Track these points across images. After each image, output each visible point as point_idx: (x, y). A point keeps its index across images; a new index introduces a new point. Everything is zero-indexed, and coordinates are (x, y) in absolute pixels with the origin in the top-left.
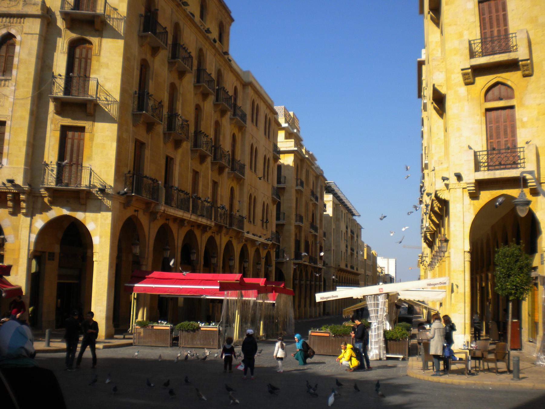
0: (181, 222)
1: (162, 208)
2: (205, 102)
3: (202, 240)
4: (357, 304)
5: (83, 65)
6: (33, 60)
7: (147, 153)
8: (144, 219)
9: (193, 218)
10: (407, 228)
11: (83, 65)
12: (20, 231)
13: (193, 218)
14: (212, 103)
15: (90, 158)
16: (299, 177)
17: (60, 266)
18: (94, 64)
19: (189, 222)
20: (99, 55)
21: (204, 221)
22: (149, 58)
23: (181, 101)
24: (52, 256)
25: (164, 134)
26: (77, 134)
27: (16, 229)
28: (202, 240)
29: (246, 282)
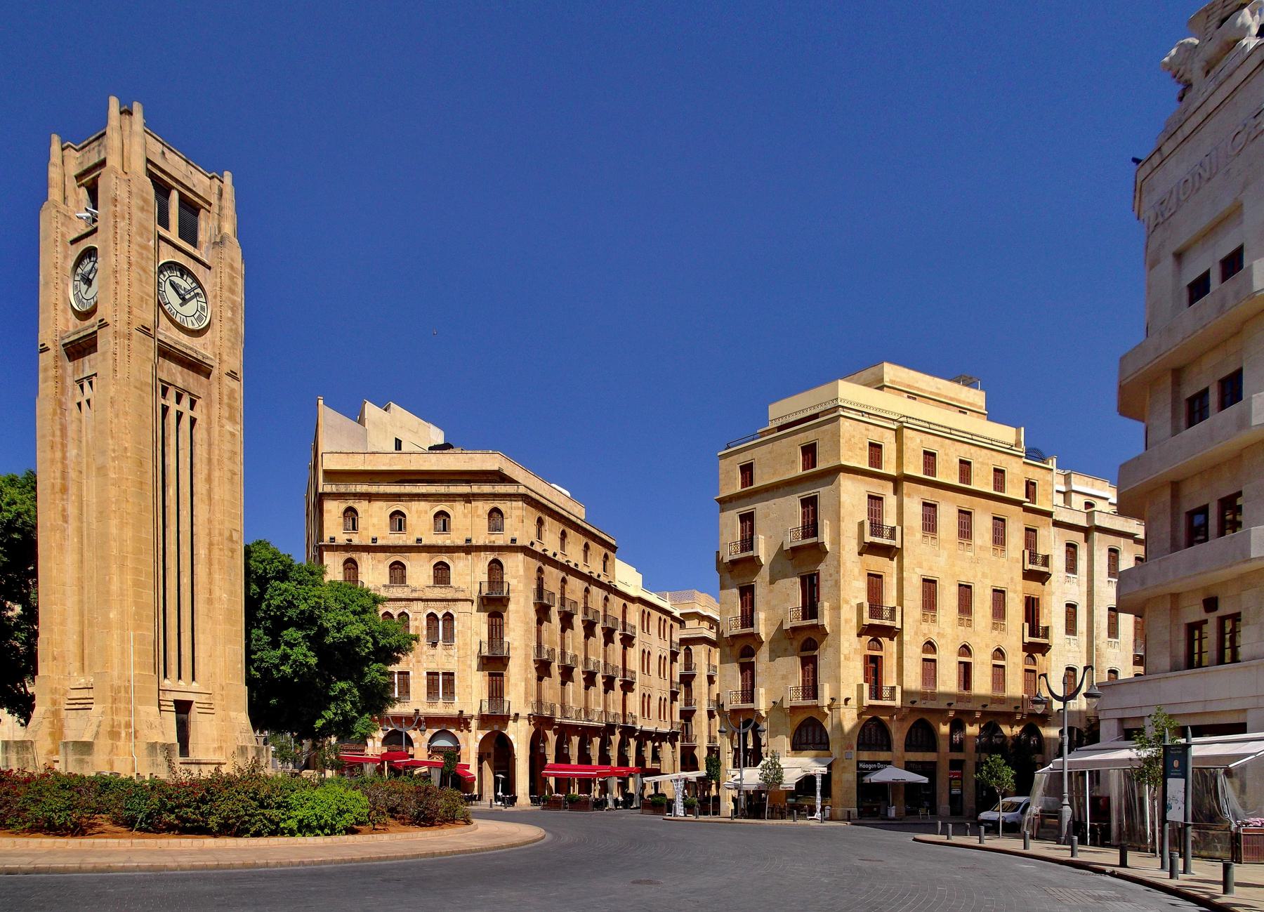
4: (821, 795)
5: (498, 630)
10: (1166, 59)
11: (498, 630)
12: (1007, 834)
15: (508, 693)
18: (506, 630)
20: (508, 623)
26: (498, 678)
27: (467, 740)
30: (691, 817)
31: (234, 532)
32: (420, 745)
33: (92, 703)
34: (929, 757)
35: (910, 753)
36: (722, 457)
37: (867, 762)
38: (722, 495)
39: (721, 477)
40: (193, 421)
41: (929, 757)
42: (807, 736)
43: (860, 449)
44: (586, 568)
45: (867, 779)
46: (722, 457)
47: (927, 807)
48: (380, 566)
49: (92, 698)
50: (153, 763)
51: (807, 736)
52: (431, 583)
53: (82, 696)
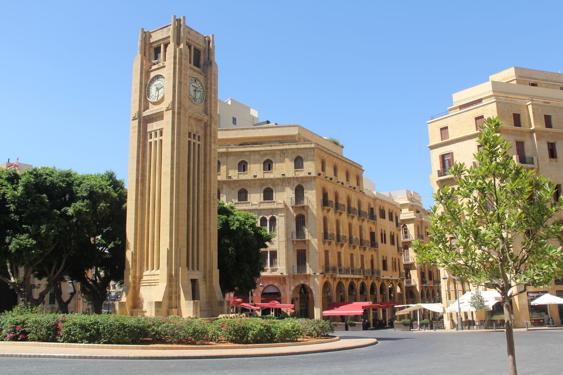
0: (347, 279)
1: (338, 275)
2: (353, 220)
3: (358, 285)
6: (284, 226)
7: (330, 254)
8: (331, 281)
9: (352, 276)
13: (352, 276)
14: (357, 219)
16: (420, 234)
17: (300, 302)
19: (350, 278)
21: (357, 276)
22: (326, 214)
23: (341, 225)
24: (297, 298)
25: (336, 243)
27: (284, 290)
28: (358, 285)
29: (497, 115)
30: (454, 330)
31: (215, 195)
32: (257, 295)
33: (158, 282)
34: (162, 46)
35: (559, 286)
36: (428, 123)
37: (533, 292)
38: (431, 144)
39: (430, 134)
40: (199, 145)
41: (162, 46)
42: (300, 220)
43: (509, 117)
44: (347, 185)
45: (532, 303)
46: (428, 123)
47: (477, 325)
48: (233, 191)
49: (158, 280)
50: (189, 311)
51: (300, 220)
52: (262, 200)
53: (150, 279)
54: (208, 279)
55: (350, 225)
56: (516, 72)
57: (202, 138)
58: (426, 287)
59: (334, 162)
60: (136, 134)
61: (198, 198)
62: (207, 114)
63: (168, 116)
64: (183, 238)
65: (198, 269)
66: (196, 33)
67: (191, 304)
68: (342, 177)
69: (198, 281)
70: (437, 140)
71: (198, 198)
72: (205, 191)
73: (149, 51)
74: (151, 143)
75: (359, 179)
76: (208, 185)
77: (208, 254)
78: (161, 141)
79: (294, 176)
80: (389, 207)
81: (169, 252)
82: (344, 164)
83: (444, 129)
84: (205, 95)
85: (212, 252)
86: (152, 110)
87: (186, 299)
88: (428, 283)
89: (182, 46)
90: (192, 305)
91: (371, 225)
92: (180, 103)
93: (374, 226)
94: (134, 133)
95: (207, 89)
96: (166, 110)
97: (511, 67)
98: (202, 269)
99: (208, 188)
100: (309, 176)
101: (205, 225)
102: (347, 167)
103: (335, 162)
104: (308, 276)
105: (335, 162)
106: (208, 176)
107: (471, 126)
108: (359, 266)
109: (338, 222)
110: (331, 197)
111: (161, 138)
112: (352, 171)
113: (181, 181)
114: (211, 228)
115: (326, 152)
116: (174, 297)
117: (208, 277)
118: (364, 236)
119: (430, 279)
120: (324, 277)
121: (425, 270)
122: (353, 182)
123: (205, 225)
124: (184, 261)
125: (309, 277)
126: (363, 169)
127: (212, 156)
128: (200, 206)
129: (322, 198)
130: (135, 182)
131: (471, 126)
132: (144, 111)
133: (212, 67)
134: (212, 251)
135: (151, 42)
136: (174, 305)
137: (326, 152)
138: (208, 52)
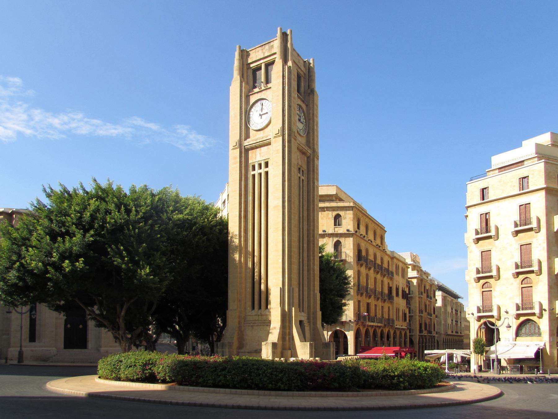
0: (372, 326)
3: (379, 331)
7: (361, 304)
38: (468, 205)
50: (305, 353)
54: (312, 321)
55: (375, 279)
56: (551, 138)
57: (305, 172)
58: (422, 336)
59: (366, 221)
60: (238, 165)
61: (303, 237)
62: (310, 147)
63: (277, 145)
64: (295, 277)
65: (303, 311)
66: (297, 55)
67: (307, 346)
68: (371, 236)
69: (304, 322)
70: (478, 200)
71: (303, 237)
72: (308, 230)
73: (247, 73)
74: (254, 176)
75: (382, 238)
76: (312, 224)
77: (312, 296)
78: (267, 173)
79: (334, 232)
80: (402, 266)
81: (282, 290)
82: (373, 224)
83: (483, 192)
84: (307, 126)
85: (316, 293)
86: (254, 138)
87: (301, 341)
88: (433, 333)
89: (290, 63)
90: (309, 347)
91: (389, 281)
92: (290, 129)
93: (391, 281)
94: (235, 163)
95: (310, 119)
96: (275, 137)
97: (549, 132)
98: (306, 311)
99: (312, 228)
100: (348, 232)
101: (308, 265)
102: (375, 227)
103: (367, 222)
104: (344, 323)
105: (367, 222)
106: (311, 214)
107: (514, 186)
108: (380, 315)
109: (367, 275)
110: (364, 253)
111: (266, 170)
112: (378, 232)
113: (292, 216)
114: (315, 269)
115: (361, 212)
116: (287, 338)
117: (312, 318)
118: (384, 290)
119: (426, 329)
120: (357, 324)
121: (422, 321)
122: (378, 242)
123: (308, 265)
124: (296, 301)
125: (345, 323)
126: (385, 229)
127: (315, 193)
128: (304, 245)
129: (357, 254)
130: (238, 218)
131: (514, 186)
132: (245, 140)
133: (314, 95)
134: (315, 292)
135: (249, 62)
136: (287, 347)
137: (361, 212)
138: (309, 80)
